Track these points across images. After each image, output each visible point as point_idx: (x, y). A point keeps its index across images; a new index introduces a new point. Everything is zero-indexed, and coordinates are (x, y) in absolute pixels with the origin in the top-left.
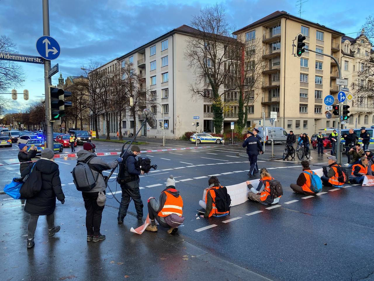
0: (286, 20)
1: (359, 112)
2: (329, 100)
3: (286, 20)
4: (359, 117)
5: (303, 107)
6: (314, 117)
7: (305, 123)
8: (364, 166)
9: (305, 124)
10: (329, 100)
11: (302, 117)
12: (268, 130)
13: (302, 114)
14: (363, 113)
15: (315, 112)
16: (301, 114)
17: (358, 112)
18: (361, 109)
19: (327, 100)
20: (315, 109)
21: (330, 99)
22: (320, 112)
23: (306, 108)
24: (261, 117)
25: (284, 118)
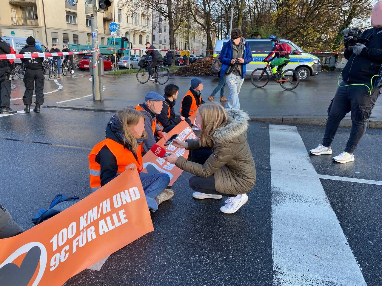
0: (137, 75)
1: (134, 31)
2: (114, 27)
3: (137, 75)
4: (134, 36)
5: (71, 16)
6: (86, 31)
7: (76, 37)
8: (128, 146)
9: (76, 39)
10: (114, 27)
11: (71, 29)
12: (14, 42)
13: (71, 25)
14: (138, 31)
15: (87, 24)
16: (69, 25)
17: (133, 30)
18: (136, 26)
19: (112, 27)
20: (87, 20)
21: (114, 26)
22: (90, 25)
23: (75, 17)
24: (12, 25)
25: (45, 28)
